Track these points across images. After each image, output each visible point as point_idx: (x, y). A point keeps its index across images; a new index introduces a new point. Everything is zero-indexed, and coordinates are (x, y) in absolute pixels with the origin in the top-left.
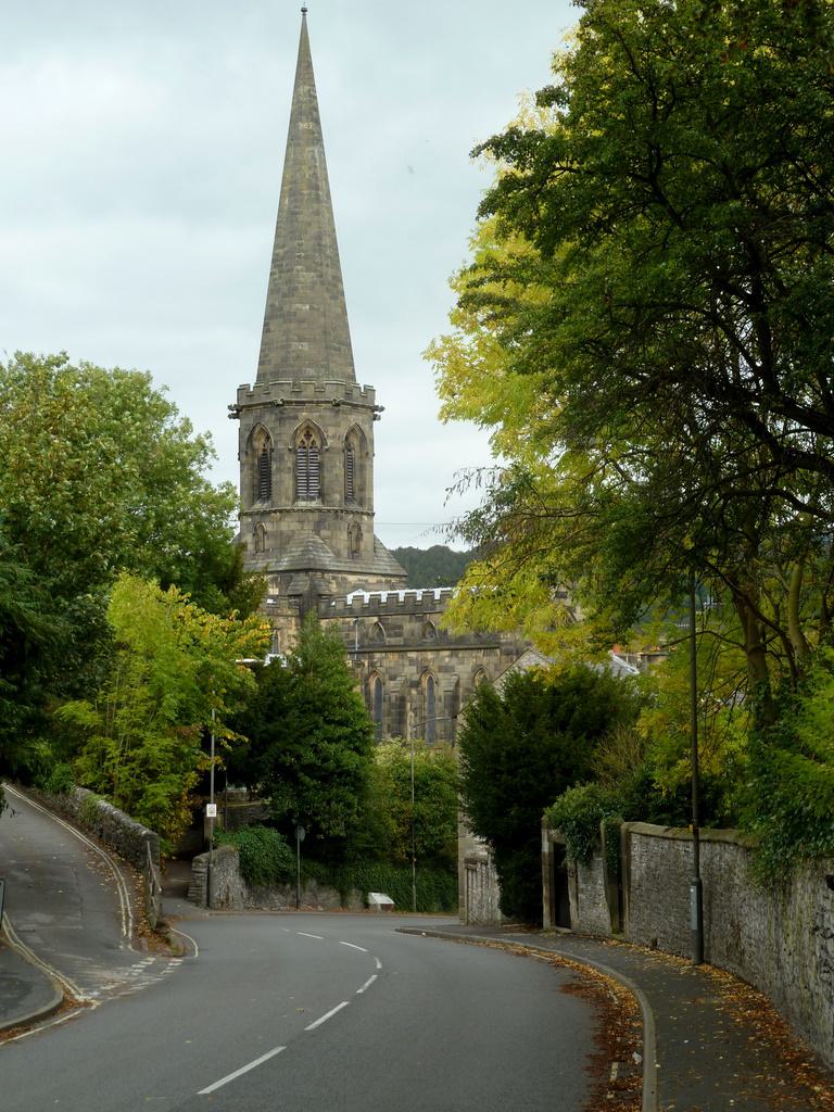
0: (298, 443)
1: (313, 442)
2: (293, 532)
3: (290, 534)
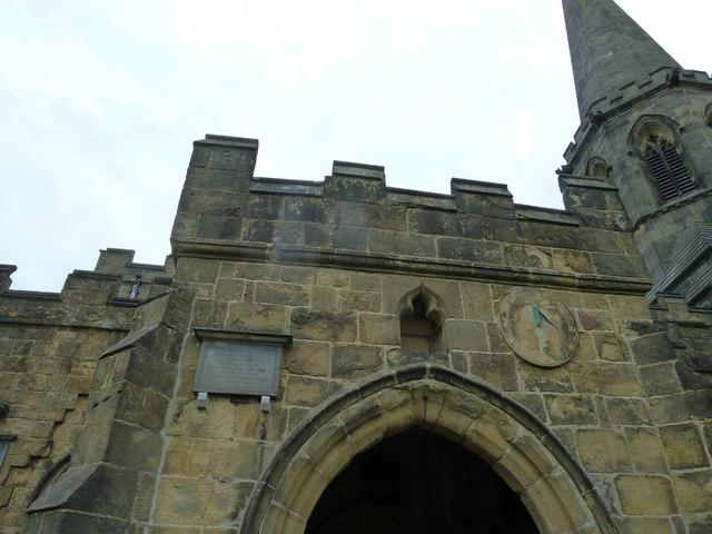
0: (643, 149)
1: (664, 141)
2: (673, 237)
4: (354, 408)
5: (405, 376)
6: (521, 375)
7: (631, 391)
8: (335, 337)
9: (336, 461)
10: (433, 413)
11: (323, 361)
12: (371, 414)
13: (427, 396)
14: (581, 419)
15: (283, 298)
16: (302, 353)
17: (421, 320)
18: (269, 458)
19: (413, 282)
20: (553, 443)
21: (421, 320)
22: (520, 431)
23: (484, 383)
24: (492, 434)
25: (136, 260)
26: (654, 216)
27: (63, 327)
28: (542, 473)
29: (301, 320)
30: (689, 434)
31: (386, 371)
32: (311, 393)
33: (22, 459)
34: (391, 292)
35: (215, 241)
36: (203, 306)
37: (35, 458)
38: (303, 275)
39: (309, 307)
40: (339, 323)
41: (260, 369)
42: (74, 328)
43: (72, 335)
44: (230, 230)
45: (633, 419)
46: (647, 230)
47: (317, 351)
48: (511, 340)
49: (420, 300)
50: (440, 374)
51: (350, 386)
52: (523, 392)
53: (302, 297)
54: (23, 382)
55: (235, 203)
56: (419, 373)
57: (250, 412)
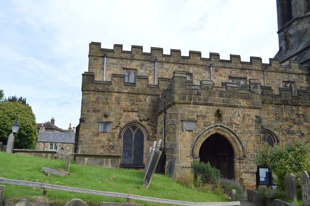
3: (305, 30)
4: (207, 132)
5: (215, 126)
6: (234, 125)
7: (252, 129)
8: (204, 120)
9: (204, 139)
10: (219, 132)
11: (202, 124)
12: (209, 133)
13: (218, 129)
14: (243, 133)
15: (194, 112)
16: (199, 123)
17: (218, 114)
18: (195, 140)
19: (217, 108)
20: (237, 137)
21: (218, 114)
22: (233, 135)
23: (228, 127)
24: (227, 135)
25: (103, 47)
26: (302, 18)
27: (114, 92)
28: (235, 142)
29: (198, 116)
30: (260, 137)
31: (212, 126)
32: (200, 130)
33: (114, 127)
34: (213, 110)
35: (182, 101)
36: (181, 114)
37: (117, 127)
38: (198, 107)
39: (199, 114)
40: (204, 117)
41: (192, 126)
42: (117, 92)
43: (118, 94)
44: (184, 98)
45: (251, 133)
46: (297, 24)
47: (201, 122)
48: (233, 119)
49: (218, 111)
50: (220, 126)
51: (206, 128)
52: (234, 129)
53: (198, 112)
54: (109, 108)
55: (184, 92)
56: (217, 126)
57: (191, 133)
